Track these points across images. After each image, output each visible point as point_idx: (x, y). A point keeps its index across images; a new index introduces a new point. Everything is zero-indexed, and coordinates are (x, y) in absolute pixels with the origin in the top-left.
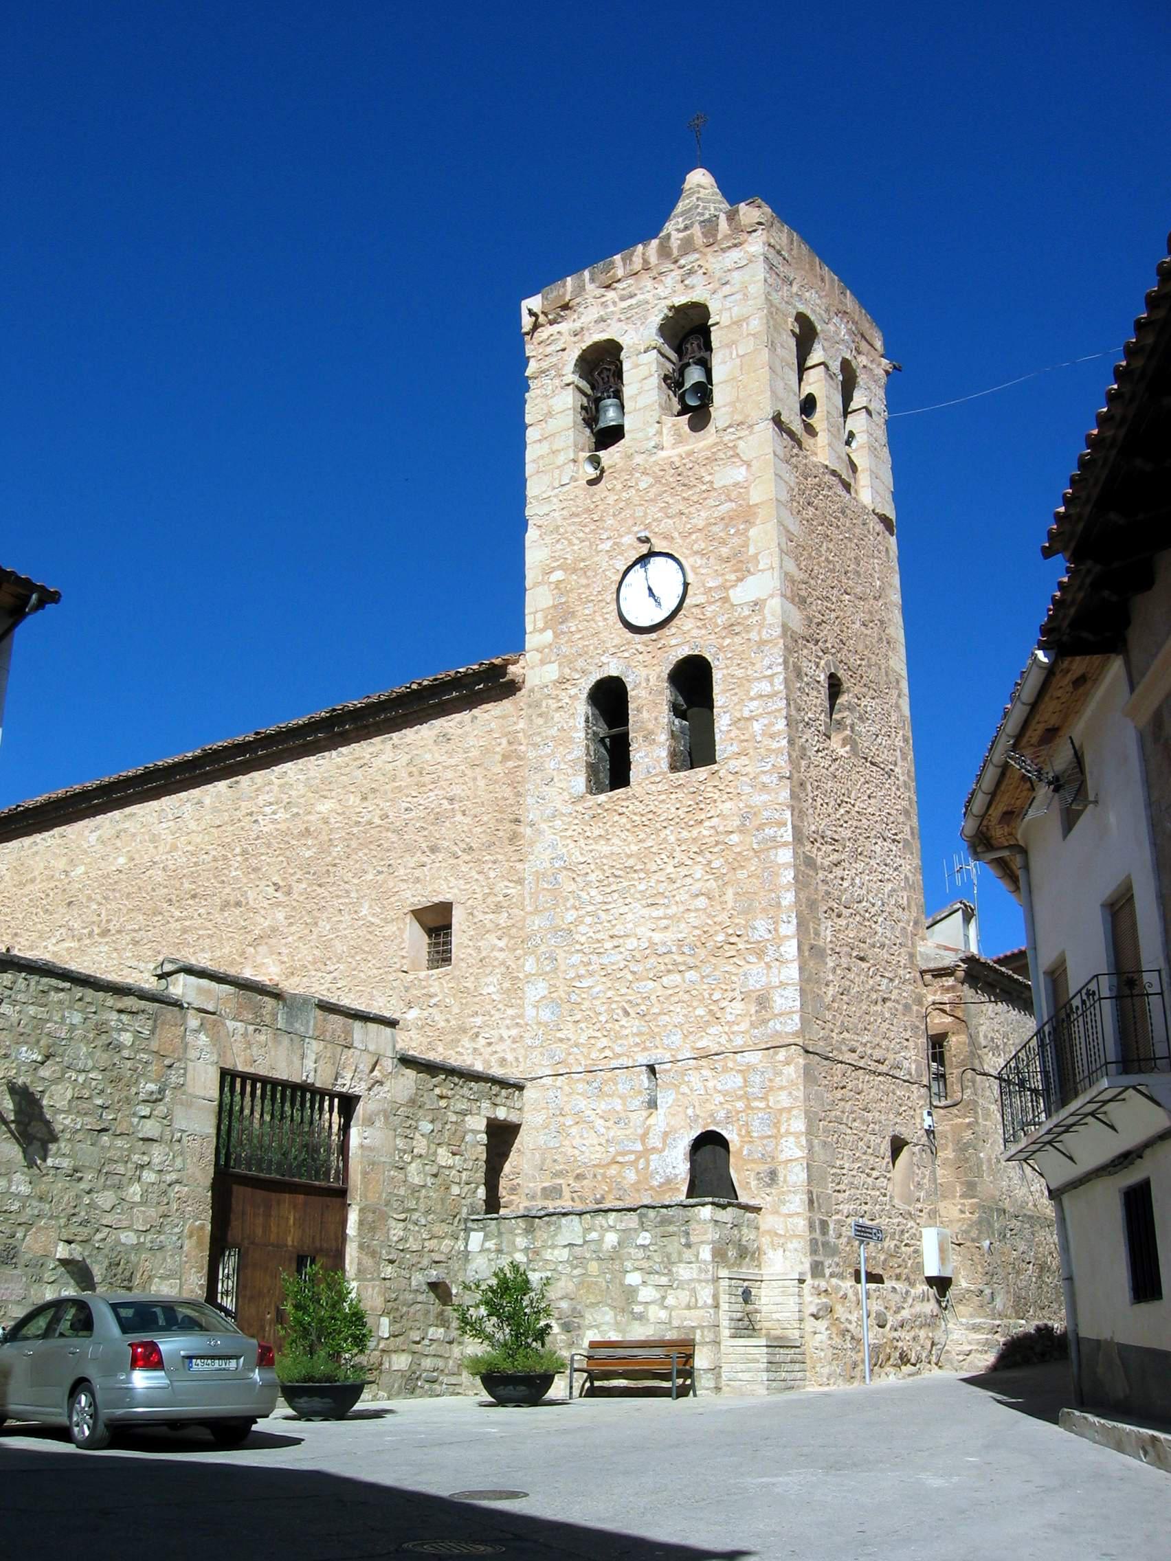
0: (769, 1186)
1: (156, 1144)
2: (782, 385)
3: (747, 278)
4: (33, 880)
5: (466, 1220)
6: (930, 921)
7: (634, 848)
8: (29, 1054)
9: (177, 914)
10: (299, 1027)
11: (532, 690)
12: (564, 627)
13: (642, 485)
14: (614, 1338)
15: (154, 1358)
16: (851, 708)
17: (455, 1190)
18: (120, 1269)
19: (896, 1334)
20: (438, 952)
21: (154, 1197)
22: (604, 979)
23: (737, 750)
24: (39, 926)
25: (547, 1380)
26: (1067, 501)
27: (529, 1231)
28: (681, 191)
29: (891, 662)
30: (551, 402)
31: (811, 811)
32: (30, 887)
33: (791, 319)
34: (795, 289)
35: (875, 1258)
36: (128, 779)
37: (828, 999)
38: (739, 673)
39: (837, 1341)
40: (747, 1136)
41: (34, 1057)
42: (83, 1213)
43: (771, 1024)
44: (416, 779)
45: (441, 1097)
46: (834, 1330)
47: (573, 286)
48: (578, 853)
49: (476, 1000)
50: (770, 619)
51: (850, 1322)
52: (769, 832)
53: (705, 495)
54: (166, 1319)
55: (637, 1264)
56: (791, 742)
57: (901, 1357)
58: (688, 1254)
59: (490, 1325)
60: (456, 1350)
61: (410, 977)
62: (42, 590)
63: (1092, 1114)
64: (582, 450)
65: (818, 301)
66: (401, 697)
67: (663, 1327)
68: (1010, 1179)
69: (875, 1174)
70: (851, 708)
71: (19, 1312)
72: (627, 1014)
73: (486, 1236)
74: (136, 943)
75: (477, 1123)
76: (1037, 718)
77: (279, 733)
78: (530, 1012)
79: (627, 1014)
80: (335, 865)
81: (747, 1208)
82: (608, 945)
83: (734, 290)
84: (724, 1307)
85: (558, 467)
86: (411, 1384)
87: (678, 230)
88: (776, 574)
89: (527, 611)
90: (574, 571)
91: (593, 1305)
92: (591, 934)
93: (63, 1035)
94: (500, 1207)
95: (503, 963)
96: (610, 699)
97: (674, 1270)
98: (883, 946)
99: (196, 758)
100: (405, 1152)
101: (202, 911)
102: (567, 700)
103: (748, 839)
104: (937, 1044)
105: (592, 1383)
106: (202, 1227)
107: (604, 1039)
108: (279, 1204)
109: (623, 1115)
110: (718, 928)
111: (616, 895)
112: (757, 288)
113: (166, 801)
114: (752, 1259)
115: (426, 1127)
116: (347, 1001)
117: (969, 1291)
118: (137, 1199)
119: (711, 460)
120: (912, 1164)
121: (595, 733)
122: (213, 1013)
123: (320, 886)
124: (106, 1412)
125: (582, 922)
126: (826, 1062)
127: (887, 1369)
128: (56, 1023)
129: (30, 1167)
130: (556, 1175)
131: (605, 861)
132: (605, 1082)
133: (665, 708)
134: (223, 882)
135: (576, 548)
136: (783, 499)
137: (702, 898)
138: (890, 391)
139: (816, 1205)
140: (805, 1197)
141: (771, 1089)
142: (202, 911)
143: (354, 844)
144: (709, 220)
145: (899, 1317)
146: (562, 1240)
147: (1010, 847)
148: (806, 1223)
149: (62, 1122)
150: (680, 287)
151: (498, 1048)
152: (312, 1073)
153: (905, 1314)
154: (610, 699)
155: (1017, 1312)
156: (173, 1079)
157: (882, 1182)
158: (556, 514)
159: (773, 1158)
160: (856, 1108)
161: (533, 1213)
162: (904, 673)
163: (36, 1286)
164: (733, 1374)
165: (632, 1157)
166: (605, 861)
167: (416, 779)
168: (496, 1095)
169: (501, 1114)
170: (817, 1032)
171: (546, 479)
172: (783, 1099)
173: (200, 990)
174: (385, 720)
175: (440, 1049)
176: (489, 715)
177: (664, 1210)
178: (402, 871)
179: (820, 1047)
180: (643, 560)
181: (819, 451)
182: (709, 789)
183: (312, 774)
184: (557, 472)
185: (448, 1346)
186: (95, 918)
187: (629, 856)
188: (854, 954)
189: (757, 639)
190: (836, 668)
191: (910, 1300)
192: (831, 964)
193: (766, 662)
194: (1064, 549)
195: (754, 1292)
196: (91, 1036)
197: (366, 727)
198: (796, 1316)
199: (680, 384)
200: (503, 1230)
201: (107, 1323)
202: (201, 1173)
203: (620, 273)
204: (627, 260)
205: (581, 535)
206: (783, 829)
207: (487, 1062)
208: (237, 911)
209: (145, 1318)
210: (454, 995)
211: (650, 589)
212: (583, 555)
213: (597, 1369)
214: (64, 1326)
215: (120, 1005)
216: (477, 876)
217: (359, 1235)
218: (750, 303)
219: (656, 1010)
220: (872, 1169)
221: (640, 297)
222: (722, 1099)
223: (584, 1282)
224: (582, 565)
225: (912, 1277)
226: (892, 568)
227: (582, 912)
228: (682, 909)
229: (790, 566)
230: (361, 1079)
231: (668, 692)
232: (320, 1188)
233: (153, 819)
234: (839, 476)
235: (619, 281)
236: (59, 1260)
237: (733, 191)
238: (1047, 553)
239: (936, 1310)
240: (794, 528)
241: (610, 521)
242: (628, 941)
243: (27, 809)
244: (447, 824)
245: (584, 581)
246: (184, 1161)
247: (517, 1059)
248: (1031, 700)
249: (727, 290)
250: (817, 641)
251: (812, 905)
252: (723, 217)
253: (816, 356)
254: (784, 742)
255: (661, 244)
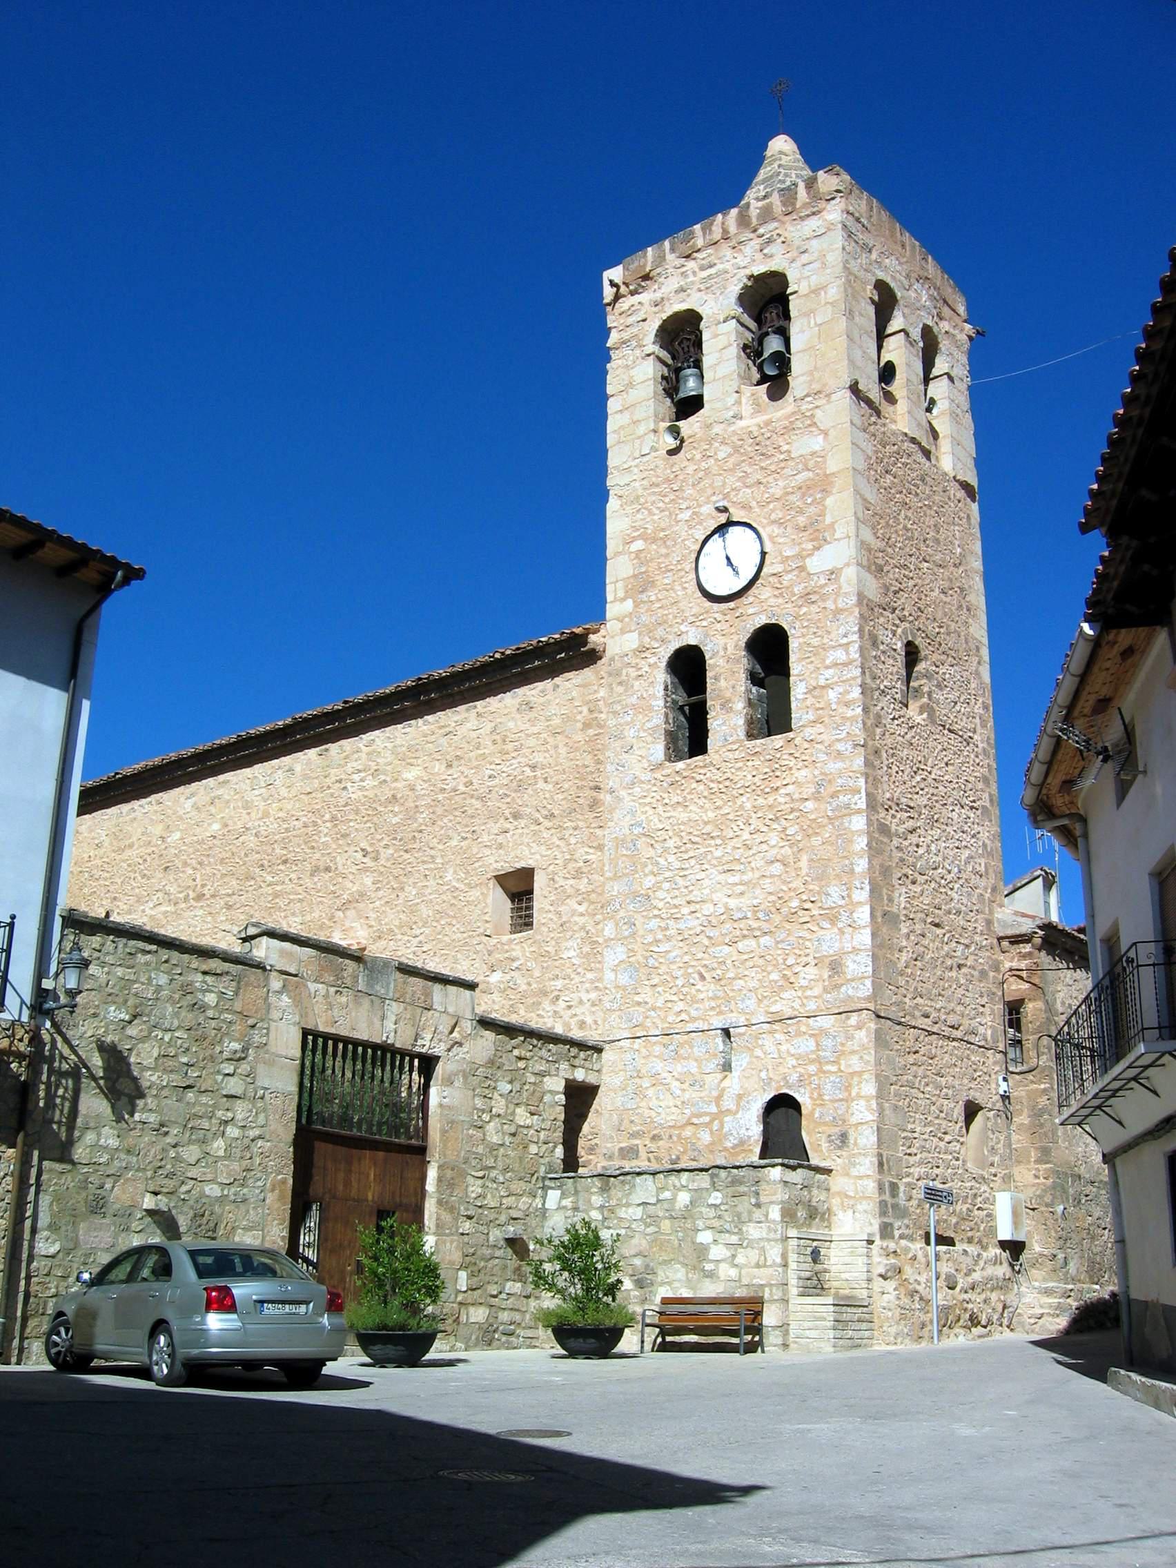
0: (840, 1148)
1: (239, 1101)
2: (859, 353)
3: (825, 246)
4: (131, 846)
5: (544, 1178)
6: (1010, 888)
7: (711, 815)
8: (116, 1014)
9: (269, 879)
10: (379, 989)
11: (612, 659)
12: (644, 597)
13: (721, 455)
14: (685, 1295)
15: (228, 1302)
16: (928, 676)
17: (533, 1149)
18: (204, 1220)
19: (966, 1296)
20: (520, 917)
21: (237, 1152)
22: (681, 944)
23: (812, 718)
24: (137, 890)
25: (616, 1334)
26: (1100, 478)
27: (605, 1189)
28: (764, 158)
29: (971, 630)
30: (633, 372)
31: (885, 778)
32: (128, 852)
33: (870, 287)
34: (874, 256)
35: (946, 1221)
36: (222, 747)
37: (901, 965)
38: (816, 642)
39: (906, 1301)
40: (819, 1099)
41: (122, 1016)
42: (169, 1166)
43: (843, 989)
44: (499, 747)
45: (520, 1058)
46: (902, 1290)
47: (654, 256)
48: (656, 820)
49: (557, 963)
50: (846, 588)
51: (919, 1284)
52: (843, 799)
53: (782, 465)
54: (244, 1266)
55: (708, 1223)
56: (866, 710)
57: (971, 1318)
58: (758, 1215)
59: (562, 1280)
60: (533, 1303)
61: (493, 941)
62: (127, 567)
63: (1135, 1079)
64: (663, 420)
65: (898, 268)
66: (485, 666)
67: (733, 1284)
68: (1087, 1145)
69: (948, 1138)
70: (928, 676)
71: (105, 1259)
72: (703, 978)
73: (563, 1194)
74: (229, 907)
75: (556, 1084)
76: (1088, 688)
77: (367, 702)
78: (609, 975)
79: (703, 978)
80: (421, 831)
81: (817, 1170)
82: (685, 910)
83: (812, 258)
84: (793, 1266)
85: (639, 438)
86: (488, 1336)
87: (758, 199)
88: (853, 542)
89: (607, 581)
90: (654, 540)
91: (665, 1262)
92: (669, 899)
93: (149, 996)
94: (578, 1167)
95: (583, 928)
96: (688, 667)
97: (744, 1229)
98: (959, 912)
99: (286, 727)
100: (483, 1111)
101: (293, 876)
102: (646, 668)
103: (822, 806)
104: (1014, 1012)
105: (664, 1339)
106: (284, 1182)
107: (681, 1003)
108: (359, 1160)
109: (698, 1077)
110: (792, 894)
111: (693, 862)
112: (835, 258)
113: (258, 768)
114: (822, 1219)
115: (505, 1087)
116: (433, 966)
117: (1041, 1255)
118: (221, 1153)
119: (789, 429)
120: (985, 1128)
121: (674, 702)
122: (296, 976)
123: (406, 851)
124: (182, 1352)
125: (660, 888)
126: (898, 1027)
127: (957, 1330)
128: (143, 984)
129: (118, 1122)
130: (633, 1135)
131: (682, 827)
132: (681, 1045)
133: (743, 676)
134: (313, 848)
135: (656, 517)
136: (860, 467)
137: (777, 864)
138: (972, 356)
139: (886, 1167)
140: (875, 1160)
141: (843, 1053)
142: (293, 876)
143: (439, 811)
144: (788, 189)
145: (970, 1279)
146: (637, 1198)
147: (1070, 816)
148: (875, 1185)
149: (149, 1078)
150: (759, 256)
151: (578, 1011)
152: (392, 1034)
153: (977, 1276)
154: (688, 667)
155: (1091, 1277)
156: (256, 1038)
157: (955, 1146)
158: (637, 484)
159: (844, 1121)
160: (929, 1073)
161: (609, 1172)
162: (985, 641)
163: (123, 1235)
164: (800, 1331)
165: (707, 1119)
166: (682, 827)
167: (499, 747)
168: (574, 1057)
169: (580, 1075)
170: (889, 996)
171: (627, 449)
172: (855, 1063)
173: (282, 953)
174: (468, 690)
175: (522, 1012)
176: (571, 683)
177: (735, 1171)
178: (485, 838)
179: (893, 1012)
180: (721, 529)
181: (899, 418)
182: (785, 757)
183: (399, 742)
184: (638, 442)
185: (525, 1301)
186: (191, 883)
187: (706, 823)
188: (929, 920)
189: (833, 607)
190: (914, 635)
191: (982, 1263)
192: (905, 931)
193: (842, 631)
194: (1102, 524)
195: (823, 1252)
196: (177, 996)
197: (451, 695)
198: (864, 1276)
199: (759, 354)
200: (579, 1188)
201: (185, 1269)
202: (284, 1130)
203: (700, 242)
204: (707, 230)
205: (661, 505)
206: (857, 797)
207: (567, 1025)
208: (327, 876)
209: (222, 1264)
210: (535, 959)
211: (728, 558)
212: (663, 525)
213: (669, 1325)
214: (146, 1273)
215: (204, 967)
216: (558, 842)
217: (438, 1191)
218: (828, 271)
219: (731, 975)
220: (945, 1133)
221: (720, 267)
222: (794, 1062)
223: (657, 1241)
224: (662, 534)
225: (985, 1240)
226: (971, 534)
227: (660, 878)
228: (757, 874)
229: (867, 535)
230: (440, 1040)
231: (745, 661)
232: (399, 1145)
233: (245, 786)
234: (919, 444)
235: (699, 250)
236: (146, 1210)
237: (815, 157)
238: (1084, 529)
239: (1009, 1274)
240: (871, 496)
241: (689, 491)
242: (705, 906)
243: (125, 777)
244: (530, 791)
245: (664, 551)
246: (267, 1118)
247: (596, 1022)
248: (1080, 672)
249: (805, 258)
250: (894, 610)
251: (886, 871)
252: (801, 186)
253: (896, 323)
254: (859, 710)
255: (740, 213)
